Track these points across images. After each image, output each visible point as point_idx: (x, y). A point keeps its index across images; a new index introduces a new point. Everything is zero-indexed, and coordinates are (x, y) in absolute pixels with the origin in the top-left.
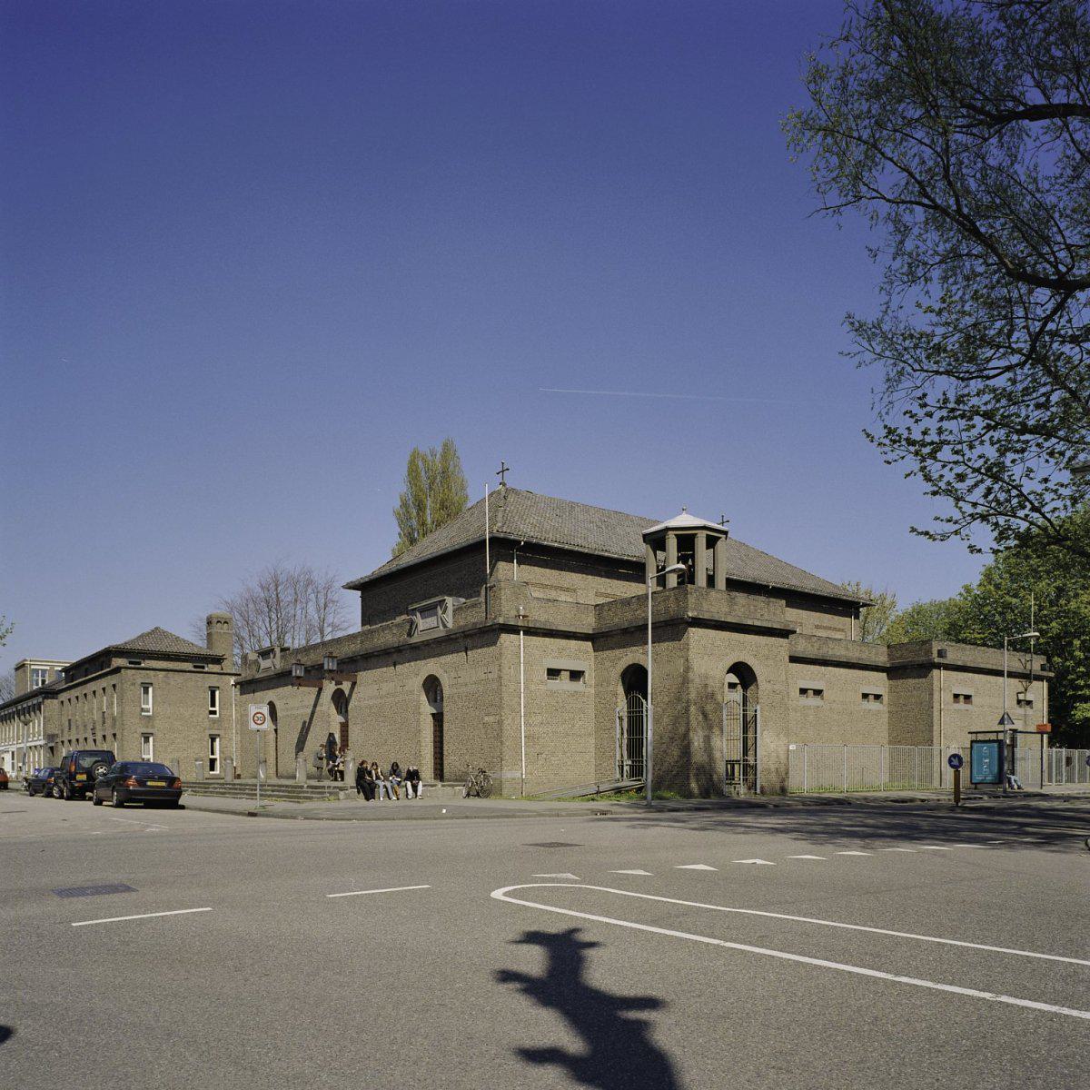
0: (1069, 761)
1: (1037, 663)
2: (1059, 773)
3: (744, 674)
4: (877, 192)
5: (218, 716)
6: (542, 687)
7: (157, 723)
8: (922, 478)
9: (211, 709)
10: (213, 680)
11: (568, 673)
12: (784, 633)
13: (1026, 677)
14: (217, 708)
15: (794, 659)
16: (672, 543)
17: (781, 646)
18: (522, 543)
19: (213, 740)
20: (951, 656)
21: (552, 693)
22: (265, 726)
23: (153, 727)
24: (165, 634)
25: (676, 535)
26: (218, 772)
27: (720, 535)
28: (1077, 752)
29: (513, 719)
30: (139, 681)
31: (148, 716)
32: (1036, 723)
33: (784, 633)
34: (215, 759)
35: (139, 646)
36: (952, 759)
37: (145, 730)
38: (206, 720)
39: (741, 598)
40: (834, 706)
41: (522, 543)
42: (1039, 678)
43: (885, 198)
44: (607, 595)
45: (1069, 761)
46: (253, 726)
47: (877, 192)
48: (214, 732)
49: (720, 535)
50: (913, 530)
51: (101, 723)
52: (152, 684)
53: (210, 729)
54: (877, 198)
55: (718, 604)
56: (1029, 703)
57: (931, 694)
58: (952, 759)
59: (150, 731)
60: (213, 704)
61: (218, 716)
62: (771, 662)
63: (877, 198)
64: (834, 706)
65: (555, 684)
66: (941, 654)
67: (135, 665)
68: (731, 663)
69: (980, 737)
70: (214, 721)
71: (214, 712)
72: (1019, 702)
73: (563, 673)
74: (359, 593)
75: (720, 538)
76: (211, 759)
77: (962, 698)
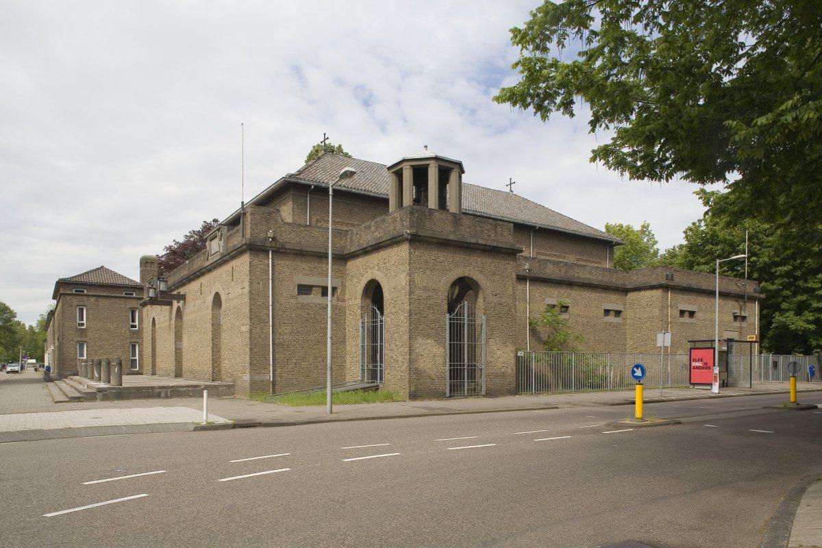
0: (775, 364)
1: (750, 288)
2: (766, 374)
5: (137, 329)
6: (293, 301)
7: (90, 335)
8: (519, 27)
10: (134, 304)
11: (320, 289)
13: (739, 297)
15: (521, 279)
17: (510, 269)
18: (313, 187)
19: (134, 347)
21: (303, 307)
23: (86, 336)
24: (107, 271)
25: (411, 166)
26: (137, 369)
27: (427, 162)
28: (781, 357)
29: (262, 328)
30: (75, 304)
31: (82, 329)
35: (84, 279)
36: (635, 369)
37: (79, 339)
38: (128, 332)
40: (579, 319)
41: (313, 187)
42: (752, 299)
45: (775, 364)
48: (135, 340)
49: (427, 162)
52: (85, 306)
53: (131, 338)
56: (744, 318)
58: (635, 369)
59: (84, 339)
60: (133, 321)
61: (137, 329)
62: (496, 278)
64: (579, 319)
65: (304, 299)
68: (455, 277)
69: (698, 345)
70: (134, 332)
71: (135, 327)
72: (736, 318)
73: (611, 312)
75: (429, 165)
76: (132, 360)
77: (687, 314)
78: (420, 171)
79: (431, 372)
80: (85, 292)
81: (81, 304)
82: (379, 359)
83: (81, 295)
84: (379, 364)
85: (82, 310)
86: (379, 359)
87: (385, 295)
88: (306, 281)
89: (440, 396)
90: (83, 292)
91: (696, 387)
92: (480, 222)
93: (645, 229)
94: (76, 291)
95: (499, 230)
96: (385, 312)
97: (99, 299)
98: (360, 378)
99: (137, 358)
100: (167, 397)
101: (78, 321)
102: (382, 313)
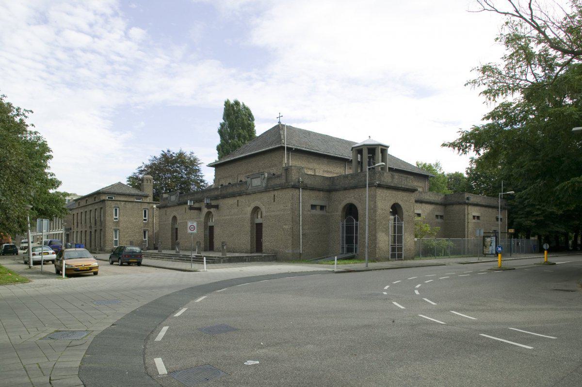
3: (396, 209)
4: (493, 8)
7: (121, 225)
9: (144, 218)
12: (413, 191)
14: (118, 217)
16: (365, 152)
17: (413, 197)
20: (472, 200)
22: (195, 231)
23: (119, 226)
27: (376, 147)
30: (113, 206)
32: (178, 228)
33: (413, 191)
34: (117, 241)
35: (112, 190)
37: (116, 228)
39: (396, 175)
43: (497, 11)
44: (338, 173)
46: (189, 231)
47: (493, 8)
48: (145, 228)
50: (32, 112)
51: (94, 224)
54: (517, 16)
55: (387, 178)
57: (465, 216)
59: (118, 228)
60: (145, 216)
63: (517, 16)
66: (468, 199)
67: (111, 199)
70: (145, 224)
71: (145, 220)
73: (317, 207)
74: (214, 168)
77: (439, 217)
78: (359, 150)
79: (383, 249)
80: (114, 199)
81: (117, 206)
82: (354, 242)
83: (111, 200)
84: (354, 245)
85: (116, 210)
86: (354, 242)
87: (359, 211)
88: (314, 203)
89: (388, 260)
90: (112, 198)
91: (487, 256)
92: (401, 176)
93: (437, 165)
94: (108, 198)
95: (408, 180)
96: (359, 220)
97: (127, 203)
98: (341, 252)
99: (118, 239)
100: (249, 261)
101: (115, 217)
102: (357, 220)
